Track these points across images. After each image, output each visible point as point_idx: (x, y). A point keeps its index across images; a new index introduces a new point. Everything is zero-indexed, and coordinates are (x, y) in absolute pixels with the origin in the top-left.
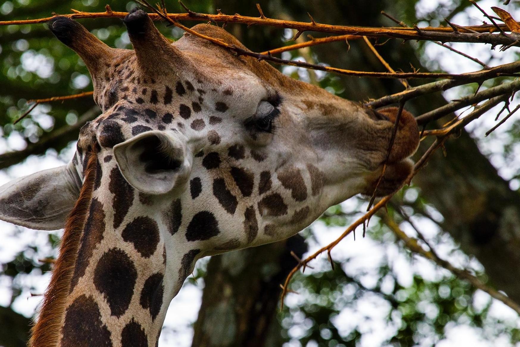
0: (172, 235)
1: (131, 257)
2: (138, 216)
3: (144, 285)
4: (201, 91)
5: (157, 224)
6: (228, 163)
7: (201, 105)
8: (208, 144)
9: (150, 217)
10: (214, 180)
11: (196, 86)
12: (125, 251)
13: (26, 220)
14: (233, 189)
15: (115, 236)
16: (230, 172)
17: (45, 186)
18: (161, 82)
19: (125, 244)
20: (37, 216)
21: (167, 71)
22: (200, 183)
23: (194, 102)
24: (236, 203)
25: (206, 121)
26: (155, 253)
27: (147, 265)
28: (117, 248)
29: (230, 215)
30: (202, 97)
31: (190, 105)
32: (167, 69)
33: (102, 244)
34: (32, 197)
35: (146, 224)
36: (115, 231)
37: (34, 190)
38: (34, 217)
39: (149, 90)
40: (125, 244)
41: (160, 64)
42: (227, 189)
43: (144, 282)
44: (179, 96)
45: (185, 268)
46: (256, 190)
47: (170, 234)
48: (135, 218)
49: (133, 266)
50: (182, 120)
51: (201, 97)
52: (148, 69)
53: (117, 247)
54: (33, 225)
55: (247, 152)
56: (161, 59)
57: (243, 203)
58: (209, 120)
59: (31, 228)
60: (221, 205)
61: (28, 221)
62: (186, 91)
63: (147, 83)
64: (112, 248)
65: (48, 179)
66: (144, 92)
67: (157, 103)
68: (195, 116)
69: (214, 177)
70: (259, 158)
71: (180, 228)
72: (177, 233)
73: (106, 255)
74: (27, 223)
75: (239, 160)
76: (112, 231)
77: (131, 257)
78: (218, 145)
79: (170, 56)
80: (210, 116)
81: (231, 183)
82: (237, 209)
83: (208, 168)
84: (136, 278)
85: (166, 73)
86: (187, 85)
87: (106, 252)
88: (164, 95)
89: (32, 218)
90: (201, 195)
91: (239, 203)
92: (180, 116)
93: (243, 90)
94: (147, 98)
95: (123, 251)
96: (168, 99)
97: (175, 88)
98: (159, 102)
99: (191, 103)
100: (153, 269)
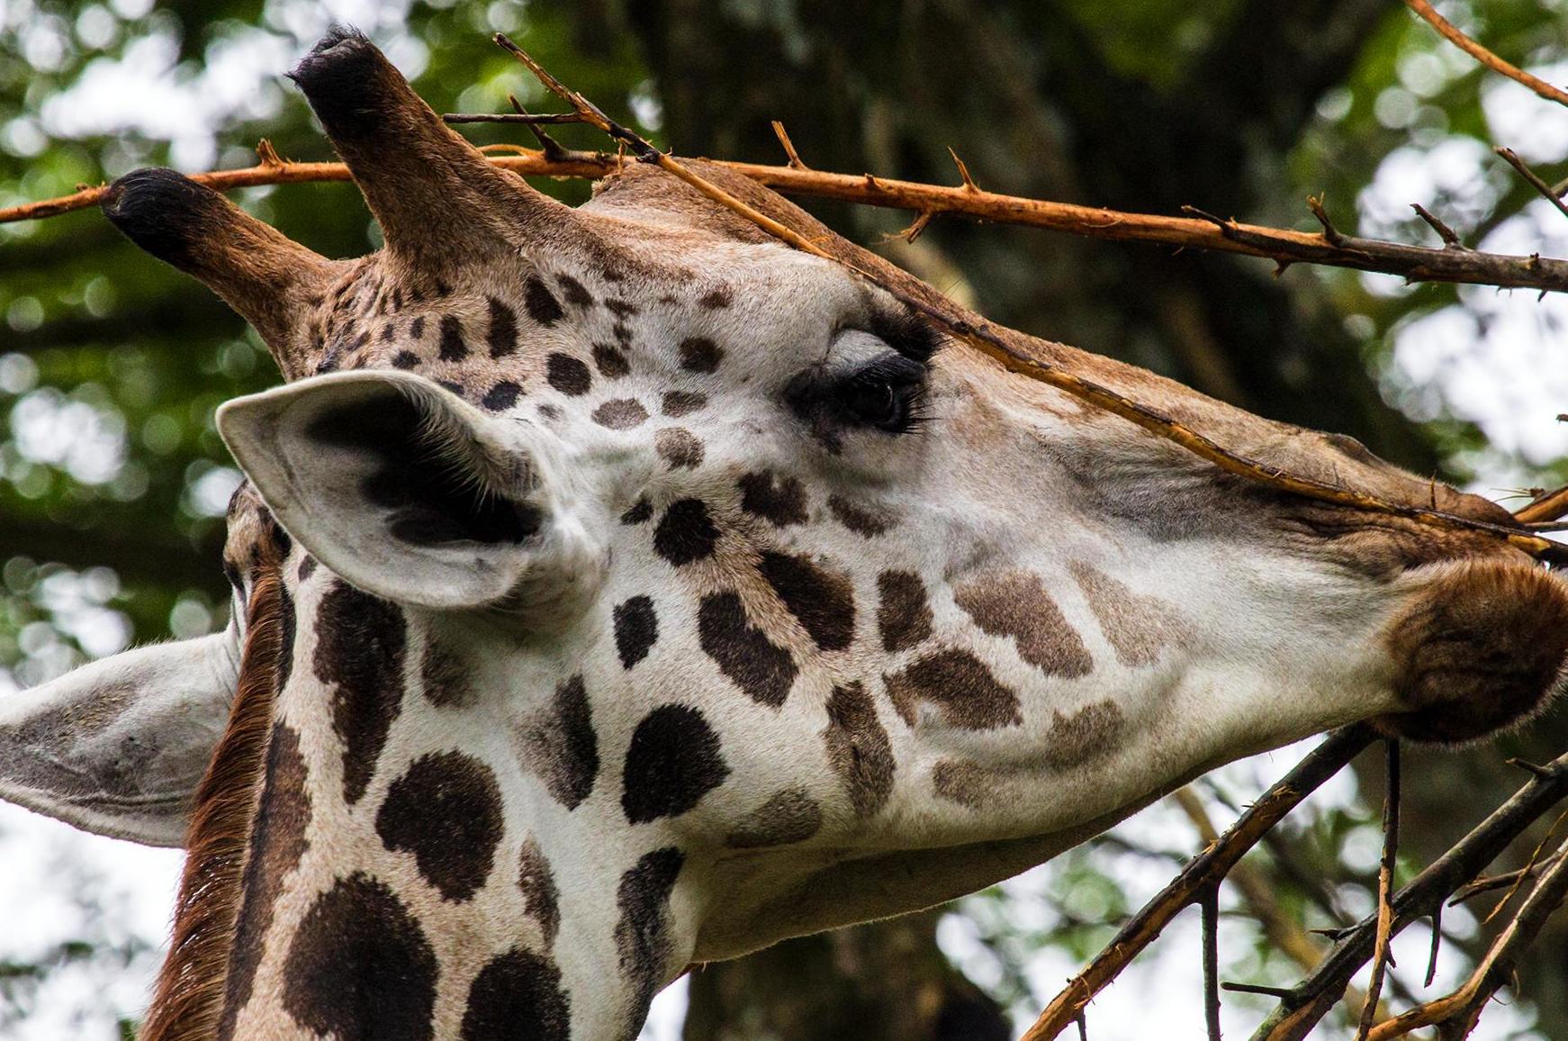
0: (571, 809)
1: (409, 904)
2: (423, 752)
3: (470, 1001)
4: (619, 308)
5: (494, 776)
6: (747, 536)
7: (625, 354)
8: (661, 465)
9: (467, 750)
10: (702, 599)
11: (599, 291)
12: (391, 886)
13: (72, 802)
14: (776, 625)
15: (353, 830)
16: (759, 567)
17: (153, 690)
18: (468, 288)
19: (389, 860)
20: (114, 789)
21: (485, 248)
22: (652, 615)
23: (598, 344)
24: (791, 671)
25: (652, 404)
26: (491, 880)
27: (467, 927)
28: (363, 874)
29: (764, 710)
30: (627, 325)
31: (585, 356)
32: (485, 238)
33: (302, 870)
34: (104, 723)
35: (451, 778)
36: (350, 812)
37: (114, 702)
38: (104, 794)
39: (432, 316)
40: (389, 858)
41: (455, 225)
42: (751, 626)
43: (465, 990)
44: (541, 329)
45: (634, 923)
46: (867, 628)
47: (563, 808)
48: (412, 761)
49: (418, 937)
50: (556, 398)
51: (621, 327)
52: (419, 250)
53: (365, 869)
54: (97, 819)
55: (816, 497)
56: (455, 206)
57: (818, 671)
58: (660, 406)
59: (87, 830)
60: (730, 680)
61: (82, 804)
62: (563, 311)
63: (424, 298)
64: (345, 875)
65: (167, 670)
66: (417, 329)
67: (464, 357)
68: (604, 389)
69: (699, 591)
70: (863, 524)
71: (598, 781)
72: (587, 800)
73: (326, 902)
74: (78, 812)
75: (787, 527)
76: (343, 814)
77: (409, 904)
78: (696, 470)
79: (489, 195)
80: (664, 390)
81: (765, 606)
82: (794, 690)
83: (677, 562)
84: (436, 977)
85: (483, 255)
86: (564, 289)
87: (325, 891)
88: (485, 330)
89: (96, 795)
90: (653, 651)
91: (801, 669)
92: (549, 385)
93: (769, 285)
94: (428, 346)
95: (385, 885)
96: (502, 338)
97: (523, 302)
98: (472, 353)
99: (589, 348)
100: (494, 940)
